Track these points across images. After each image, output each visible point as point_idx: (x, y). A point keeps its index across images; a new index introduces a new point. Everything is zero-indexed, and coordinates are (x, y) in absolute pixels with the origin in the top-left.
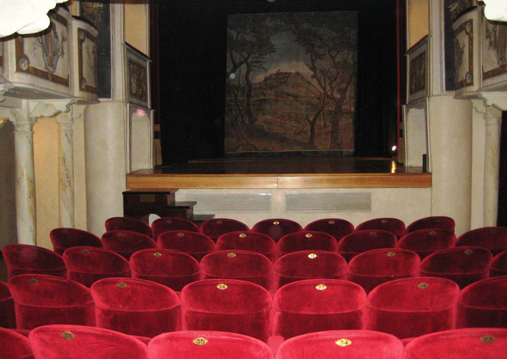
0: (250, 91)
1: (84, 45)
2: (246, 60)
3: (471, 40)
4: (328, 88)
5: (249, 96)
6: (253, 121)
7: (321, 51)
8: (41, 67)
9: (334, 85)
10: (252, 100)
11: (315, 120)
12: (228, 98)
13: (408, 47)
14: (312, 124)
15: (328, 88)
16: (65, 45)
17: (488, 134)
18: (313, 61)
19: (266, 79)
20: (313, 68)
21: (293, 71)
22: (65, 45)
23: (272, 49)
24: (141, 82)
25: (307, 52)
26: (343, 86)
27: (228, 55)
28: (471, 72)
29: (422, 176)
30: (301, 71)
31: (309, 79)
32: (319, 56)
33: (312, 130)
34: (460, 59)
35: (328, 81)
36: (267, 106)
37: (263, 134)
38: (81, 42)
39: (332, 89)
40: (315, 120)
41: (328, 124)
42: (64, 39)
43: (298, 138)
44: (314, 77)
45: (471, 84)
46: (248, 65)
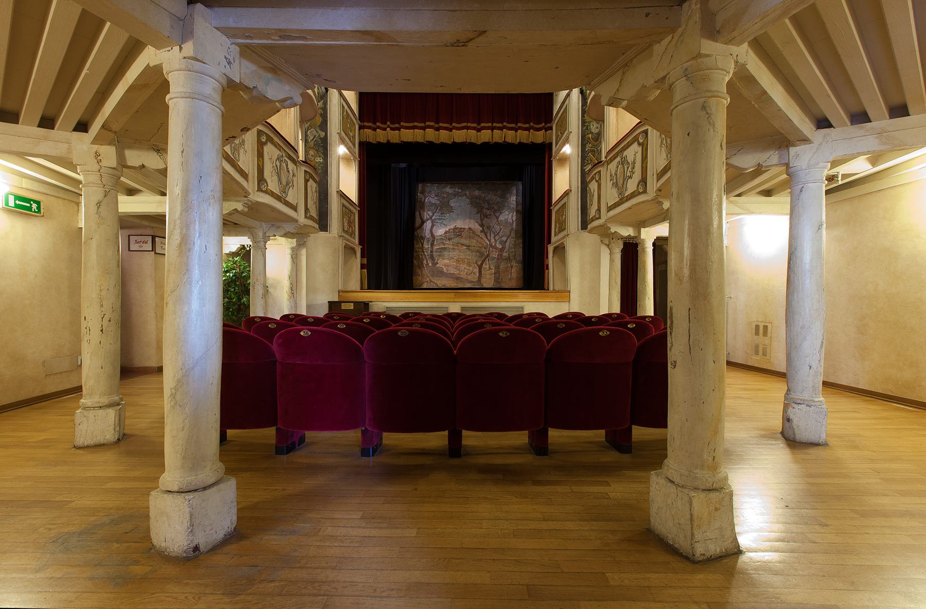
0: (433, 241)
1: (309, 184)
2: (431, 218)
3: (599, 186)
4: (493, 240)
5: (432, 245)
6: (435, 264)
7: (488, 212)
8: (277, 191)
9: (497, 238)
10: (435, 248)
11: (482, 264)
12: (416, 246)
13: (554, 201)
14: (480, 267)
15: (493, 240)
16: (295, 179)
17: (612, 261)
18: (482, 220)
19: (446, 233)
20: (482, 225)
21: (467, 227)
22: (295, 179)
23: (451, 210)
24: (350, 223)
25: (477, 213)
26: (504, 239)
27: (417, 213)
28: (599, 210)
29: (564, 294)
30: (473, 227)
31: (479, 233)
32: (486, 216)
33: (480, 272)
34: (591, 201)
35: (492, 235)
36: (446, 253)
37: (441, 273)
38: (306, 181)
39: (496, 241)
40: (482, 264)
41: (492, 267)
42: (294, 175)
43: (469, 277)
44: (481, 231)
45: (600, 218)
46: (432, 222)
